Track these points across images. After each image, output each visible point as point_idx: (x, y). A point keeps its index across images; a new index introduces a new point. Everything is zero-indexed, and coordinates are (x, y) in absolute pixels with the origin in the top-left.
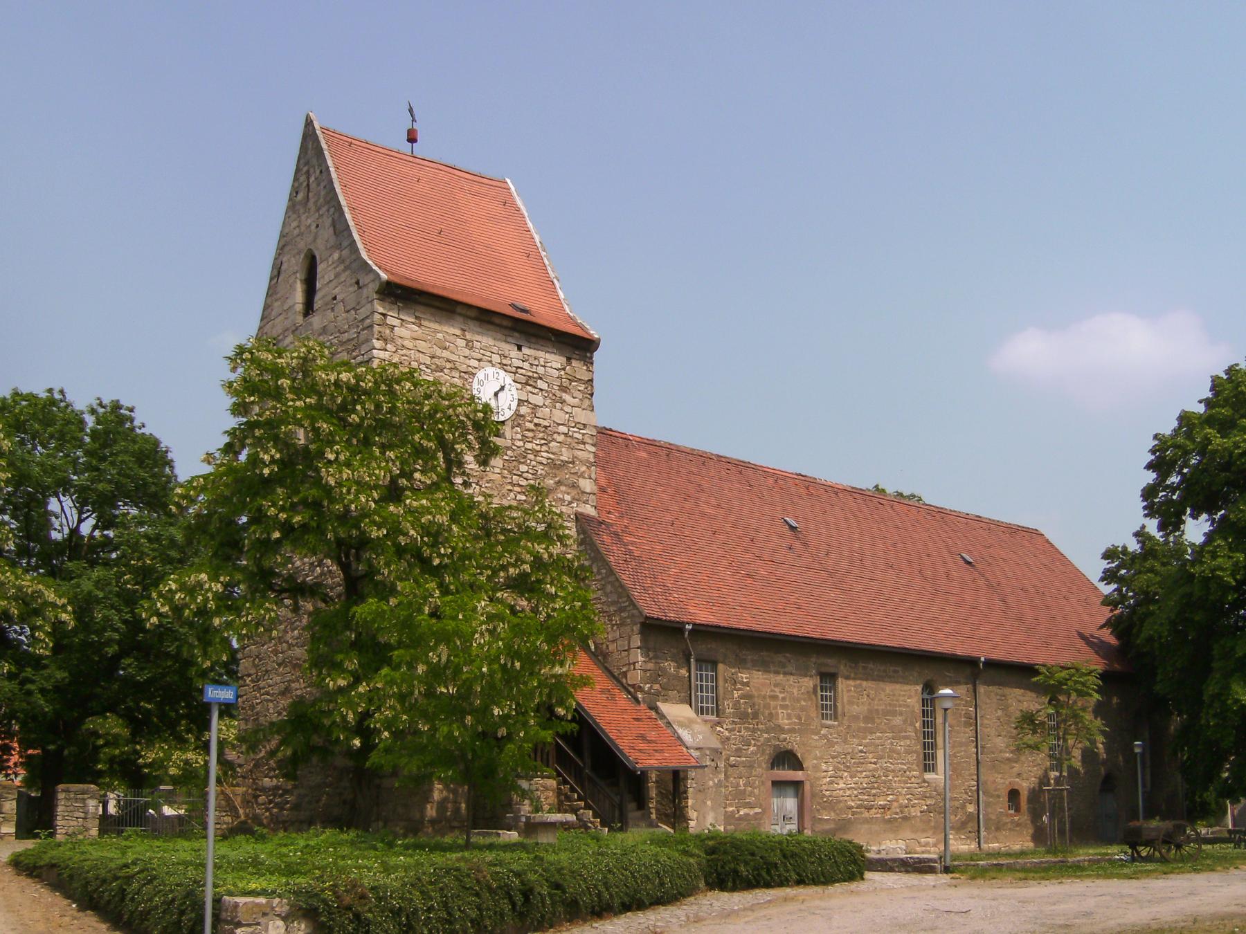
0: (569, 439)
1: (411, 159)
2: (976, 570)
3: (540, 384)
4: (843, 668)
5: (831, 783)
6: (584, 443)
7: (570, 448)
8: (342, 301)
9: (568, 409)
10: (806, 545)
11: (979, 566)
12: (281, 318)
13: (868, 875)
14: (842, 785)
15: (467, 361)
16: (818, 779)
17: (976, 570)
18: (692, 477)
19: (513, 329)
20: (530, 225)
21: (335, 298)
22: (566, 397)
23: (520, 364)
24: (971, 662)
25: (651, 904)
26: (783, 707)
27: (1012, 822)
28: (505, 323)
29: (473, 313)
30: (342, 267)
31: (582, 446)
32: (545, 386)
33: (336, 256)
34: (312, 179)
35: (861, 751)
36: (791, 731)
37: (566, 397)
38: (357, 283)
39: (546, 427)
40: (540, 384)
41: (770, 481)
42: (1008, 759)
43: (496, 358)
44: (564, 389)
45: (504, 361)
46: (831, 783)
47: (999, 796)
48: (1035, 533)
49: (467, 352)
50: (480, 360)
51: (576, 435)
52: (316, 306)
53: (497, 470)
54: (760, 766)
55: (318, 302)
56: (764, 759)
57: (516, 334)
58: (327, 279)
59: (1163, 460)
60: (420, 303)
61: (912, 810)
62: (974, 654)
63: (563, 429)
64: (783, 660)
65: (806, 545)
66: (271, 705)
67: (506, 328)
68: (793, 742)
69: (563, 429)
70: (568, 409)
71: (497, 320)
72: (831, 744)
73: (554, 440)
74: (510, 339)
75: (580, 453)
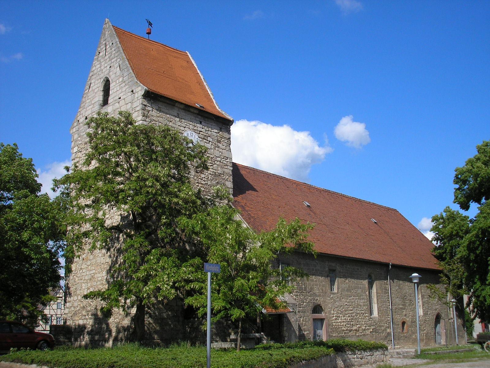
0: (221, 164)
1: (149, 41)
2: (378, 226)
3: (209, 139)
4: (338, 268)
5: (336, 319)
6: (227, 166)
7: (222, 168)
8: (124, 99)
9: (221, 150)
10: (315, 213)
11: (379, 224)
12: (91, 107)
13: (37, 349)
14: (340, 320)
15: (180, 128)
16: (331, 318)
17: (378, 226)
18: (265, 183)
19: (198, 114)
20: (199, 72)
21: (120, 98)
22: (220, 145)
23: (201, 130)
24: (386, 265)
25: (25, 363)
26: (317, 285)
27: (404, 336)
28: (195, 111)
29: (182, 106)
30: (124, 84)
31: (226, 167)
32: (211, 140)
33: (121, 79)
34: (108, 47)
35: (346, 305)
36: (319, 296)
37: (220, 145)
38: (132, 91)
39: (212, 158)
40: (209, 139)
41: (295, 186)
42: (401, 308)
43: (191, 127)
44: (219, 142)
45: (195, 128)
46: (336, 319)
47: (398, 325)
48: (395, 210)
49: (179, 124)
50: (185, 127)
51: (224, 162)
52: (109, 102)
53: (192, 177)
54: (308, 312)
55: (110, 100)
56: (310, 308)
57: (200, 117)
58: (115, 90)
59: (460, 179)
60: (161, 101)
61: (367, 331)
62: (387, 262)
63: (219, 159)
64: (315, 263)
65: (315, 213)
66: (83, 285)
67: (195, 114)
68: (320, 300)
69: (219, 159)
70: (221, 150)
71: (192, 110)
72: (335, 301)
73: (215, 164)
74: (197, 119)
75: (226, 170)
